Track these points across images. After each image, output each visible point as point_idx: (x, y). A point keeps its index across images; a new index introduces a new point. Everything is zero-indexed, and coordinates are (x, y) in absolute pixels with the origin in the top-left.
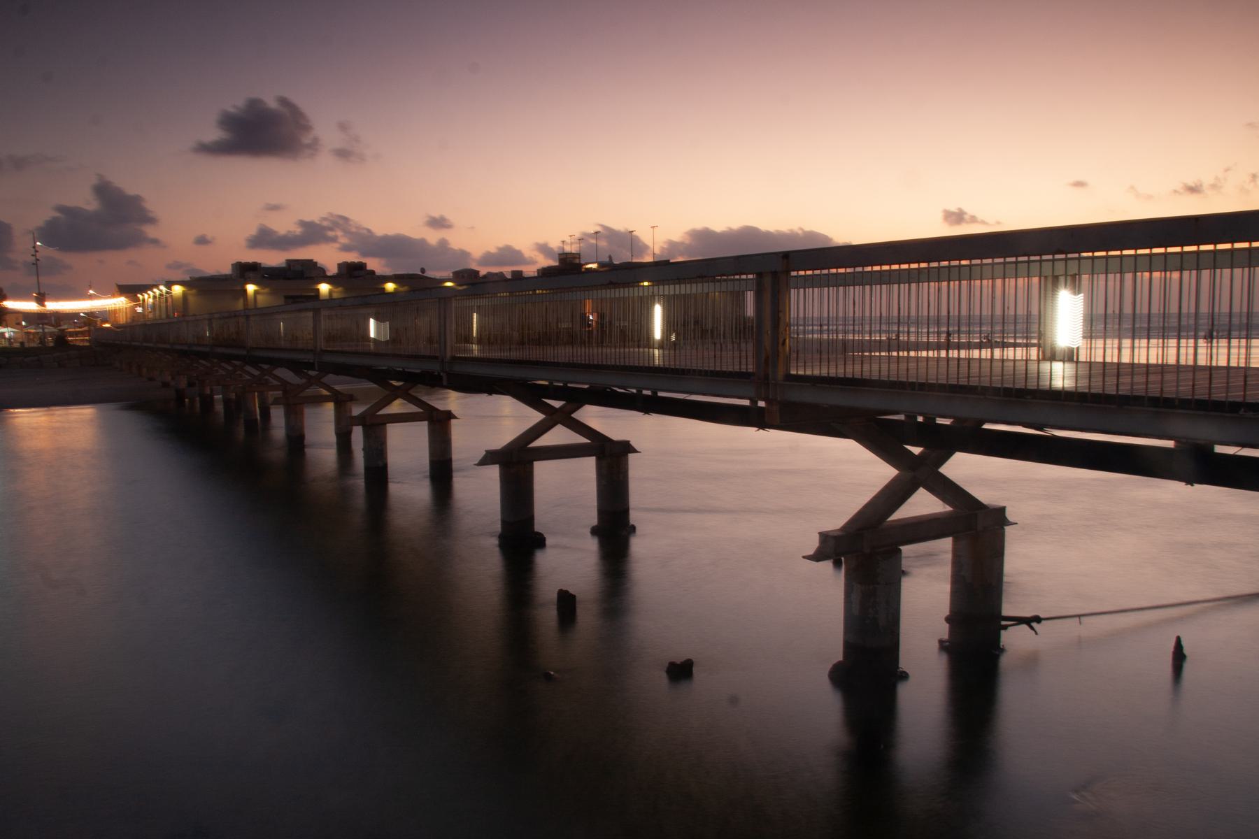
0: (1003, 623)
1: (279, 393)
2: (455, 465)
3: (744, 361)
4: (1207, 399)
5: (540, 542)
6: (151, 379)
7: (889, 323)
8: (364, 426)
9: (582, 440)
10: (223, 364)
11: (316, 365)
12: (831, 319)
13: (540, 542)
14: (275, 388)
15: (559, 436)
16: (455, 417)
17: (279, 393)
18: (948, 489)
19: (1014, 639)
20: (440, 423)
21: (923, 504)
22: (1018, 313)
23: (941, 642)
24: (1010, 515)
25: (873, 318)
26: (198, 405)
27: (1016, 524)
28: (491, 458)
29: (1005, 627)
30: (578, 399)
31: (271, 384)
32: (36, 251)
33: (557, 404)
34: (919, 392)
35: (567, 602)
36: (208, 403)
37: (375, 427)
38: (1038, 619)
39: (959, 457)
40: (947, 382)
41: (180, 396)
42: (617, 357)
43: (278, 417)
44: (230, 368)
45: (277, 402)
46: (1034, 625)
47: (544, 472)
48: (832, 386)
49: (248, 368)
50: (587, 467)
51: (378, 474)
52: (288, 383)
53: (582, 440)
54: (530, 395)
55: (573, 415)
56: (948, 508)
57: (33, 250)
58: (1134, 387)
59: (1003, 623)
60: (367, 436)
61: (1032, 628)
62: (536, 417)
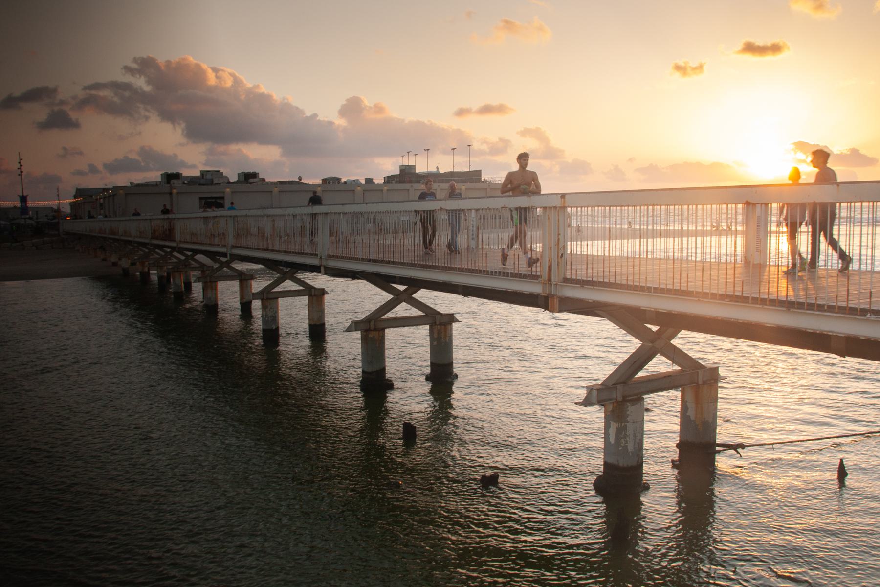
0: (717, 448)
1: (198, 273)
2: (282, 331)
3: (470, 263)
4: (846, 306)
5: (389, 386)
6: (104, 260)
7: (778, 265)
8: (262, 300)
9: (420, 313)
10: (157, 250)
11: (228, 255)
12: (642, 254)
13: (389, 386)
14: (194, 269)
15: (403, 310)
16: (328, 294)
17: (198, 273)
18: (675, 355)
19: (724, 463)
20: (316, 296)
21: (659, 365)
22: (639, 240)
23: (673, 461)
24: (722, 372)
25: (642, 251)
26: (172, 280)
27: (576, 403)
28: (355, 326)
29: (719, 452)
30: (416, 284)
31: (192, 266)
32: (21, 166)
33: (402, 288)
34: (654, 294)
35: (410, 432)
36: (146, 276)
37: (269, 297)
38: (742, 446)
39: (683, 333)
40: (673, 287)
41: (126, 272)
42: (730, 280)
43: (197, 288)
44: (147, 251)
45: (198, 280)
46: (739, 450)
47: (392, 335)
48: (595, 287)
49: (175, 254)
50: (424, 331)
51: (272, 335)
52: (206, 265)
53: (420, 313)
54: (382, 281)
55: (413, 296)
56: (680, 368)
57: (22, 164)
58: (151, 272)
59: (717, 448)
60: (264, 307)
61: (738, 453)
62: (387, 297)
